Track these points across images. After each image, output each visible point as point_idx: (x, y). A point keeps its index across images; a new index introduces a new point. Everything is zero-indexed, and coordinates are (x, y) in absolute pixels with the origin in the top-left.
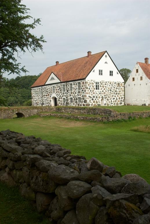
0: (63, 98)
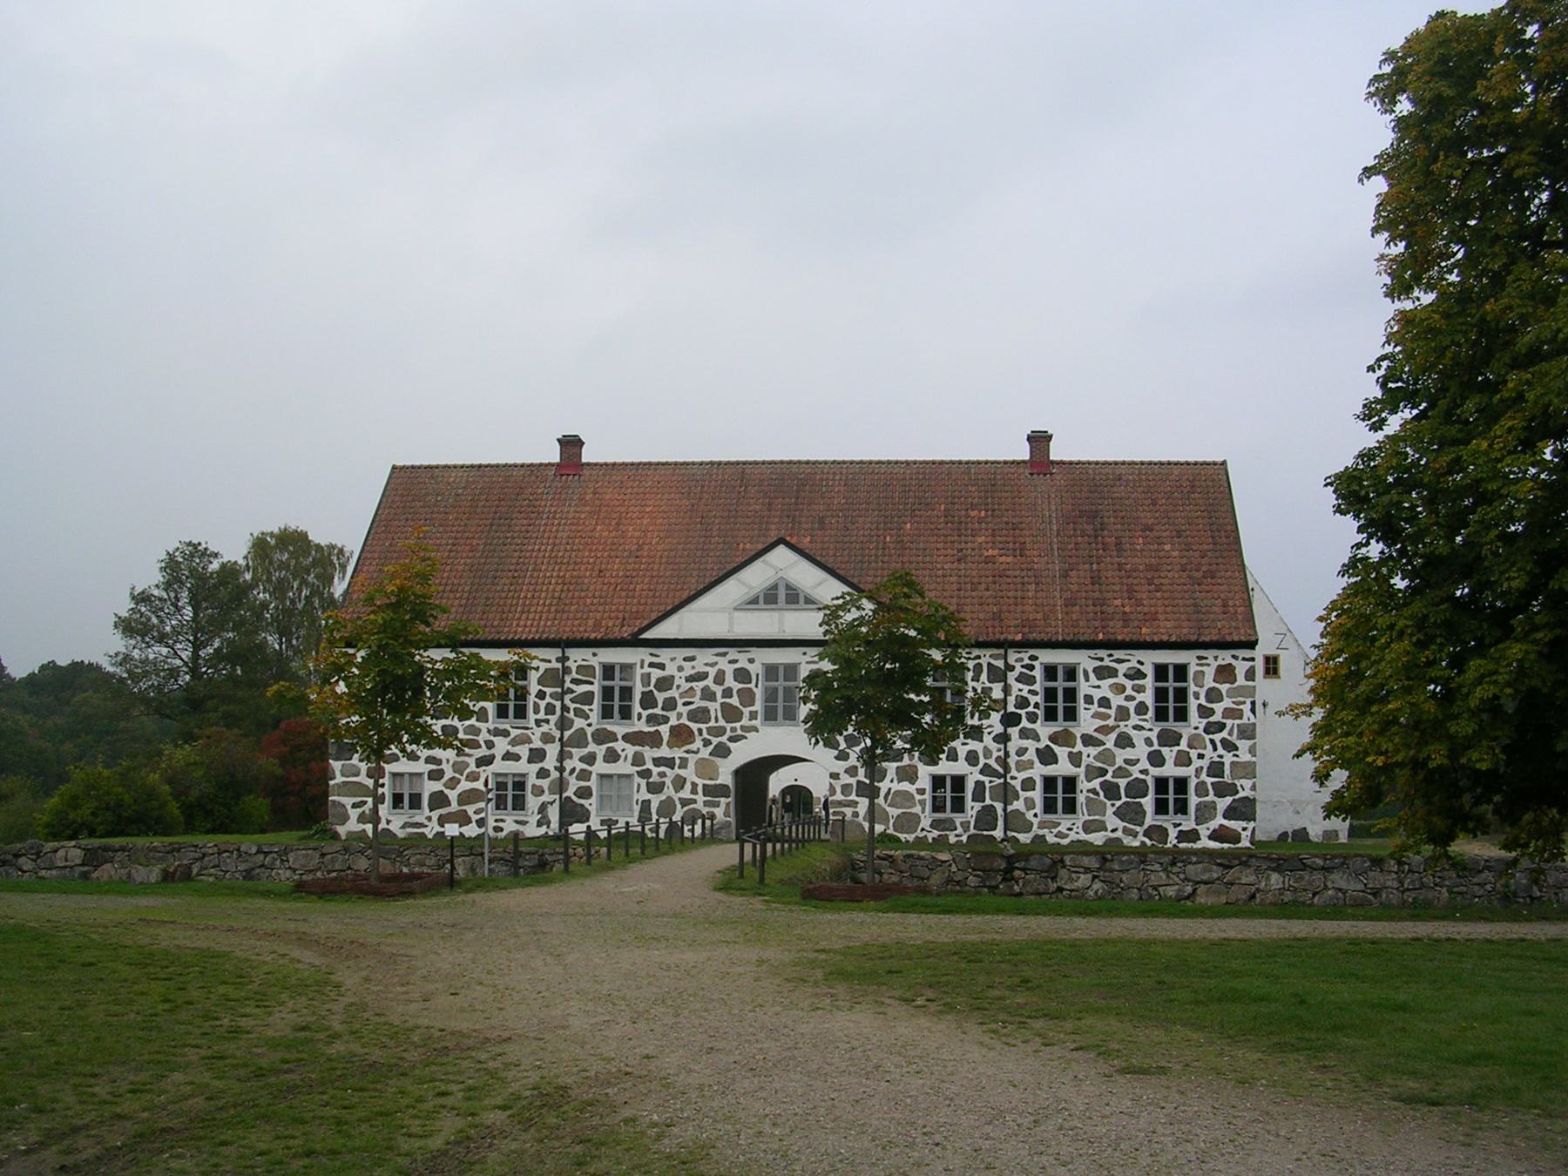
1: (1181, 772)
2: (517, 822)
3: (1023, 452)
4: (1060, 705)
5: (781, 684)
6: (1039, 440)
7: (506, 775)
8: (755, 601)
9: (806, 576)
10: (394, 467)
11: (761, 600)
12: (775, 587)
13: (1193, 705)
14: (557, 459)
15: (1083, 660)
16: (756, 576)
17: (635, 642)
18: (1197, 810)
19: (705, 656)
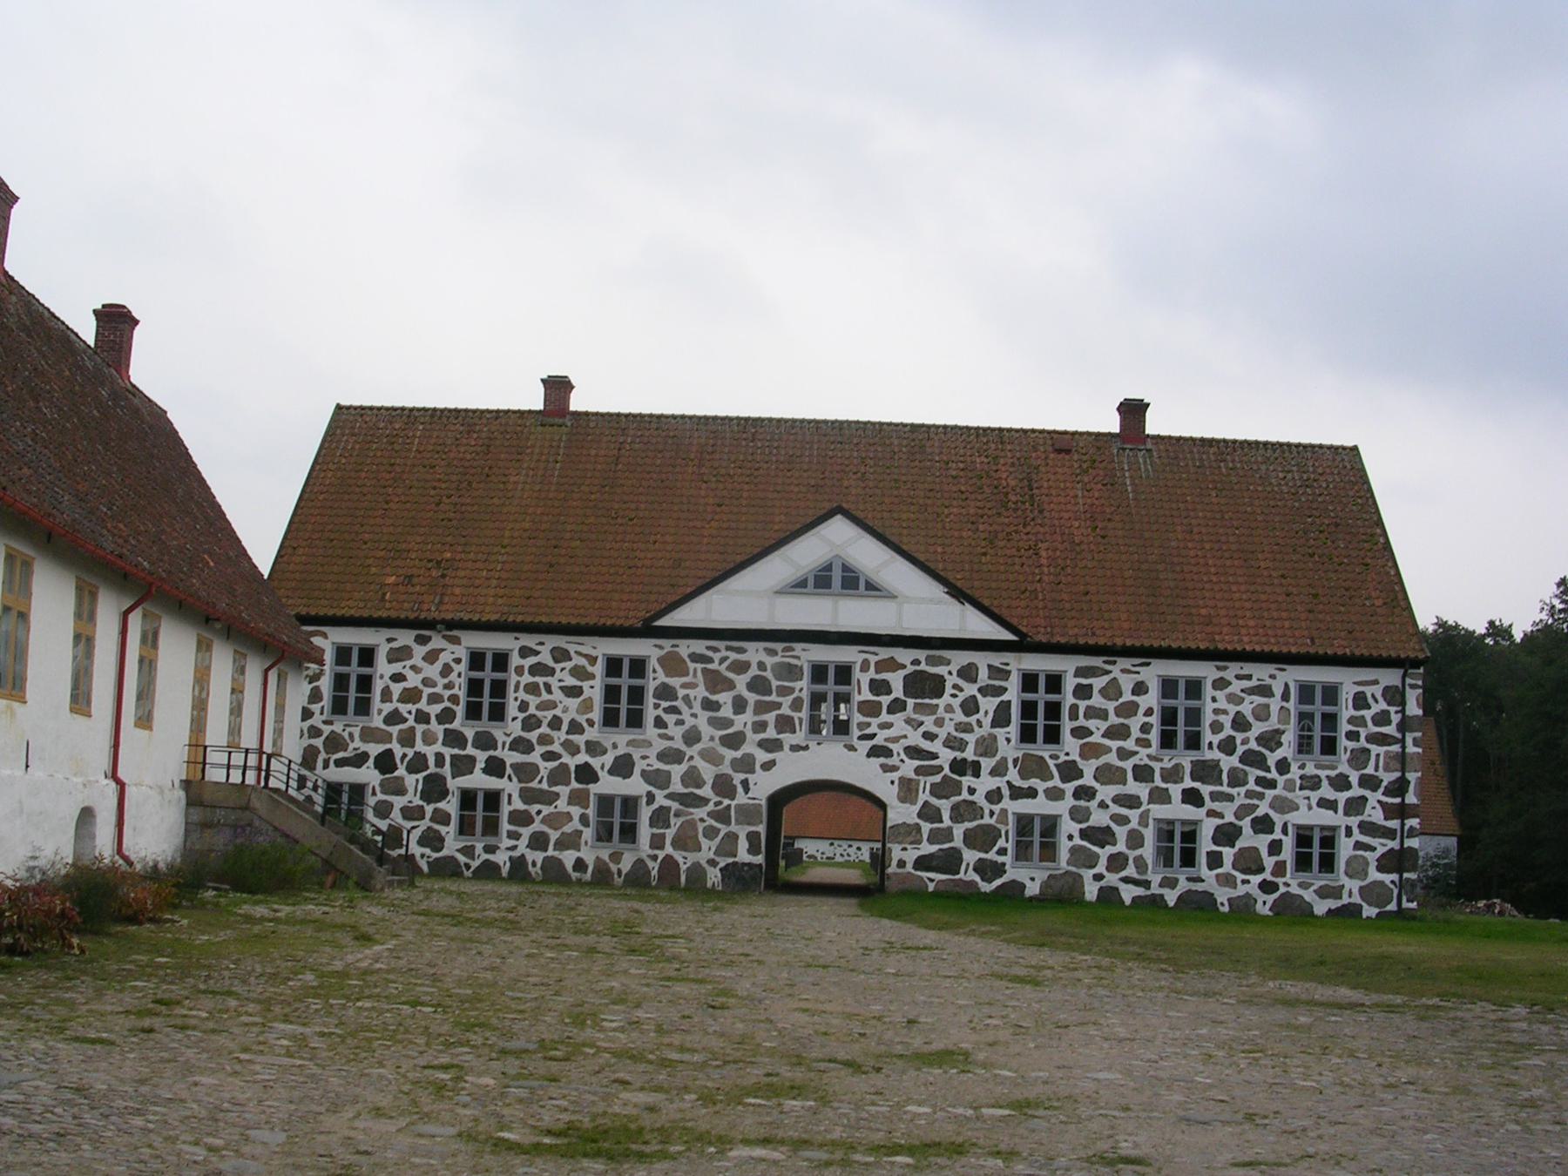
0: (468, 798)
1: (492, 783)
2: (1189, 879)
3: (534, 400)
4: (1041, 722)
5: (625, 681)
6: (1133, 411)
7: (1311, 828)
8: (801, 584)
9: (868, 554)
10: (1355, 448)
11: (811, 582)
12: (828, 567)
13: (1067, 725)
14: (539, 406)
15: (1066, 665)
16: (807, 552)
17: (648, 630)
18: (1348, 863)
19: (755, 653)
